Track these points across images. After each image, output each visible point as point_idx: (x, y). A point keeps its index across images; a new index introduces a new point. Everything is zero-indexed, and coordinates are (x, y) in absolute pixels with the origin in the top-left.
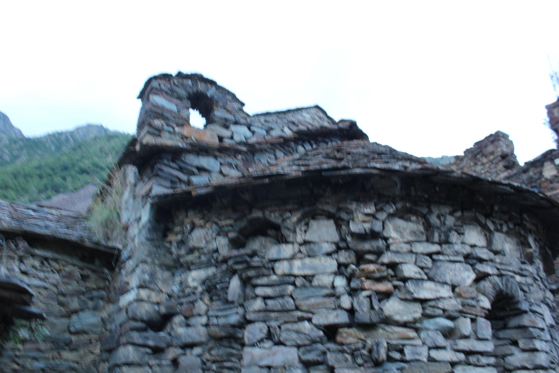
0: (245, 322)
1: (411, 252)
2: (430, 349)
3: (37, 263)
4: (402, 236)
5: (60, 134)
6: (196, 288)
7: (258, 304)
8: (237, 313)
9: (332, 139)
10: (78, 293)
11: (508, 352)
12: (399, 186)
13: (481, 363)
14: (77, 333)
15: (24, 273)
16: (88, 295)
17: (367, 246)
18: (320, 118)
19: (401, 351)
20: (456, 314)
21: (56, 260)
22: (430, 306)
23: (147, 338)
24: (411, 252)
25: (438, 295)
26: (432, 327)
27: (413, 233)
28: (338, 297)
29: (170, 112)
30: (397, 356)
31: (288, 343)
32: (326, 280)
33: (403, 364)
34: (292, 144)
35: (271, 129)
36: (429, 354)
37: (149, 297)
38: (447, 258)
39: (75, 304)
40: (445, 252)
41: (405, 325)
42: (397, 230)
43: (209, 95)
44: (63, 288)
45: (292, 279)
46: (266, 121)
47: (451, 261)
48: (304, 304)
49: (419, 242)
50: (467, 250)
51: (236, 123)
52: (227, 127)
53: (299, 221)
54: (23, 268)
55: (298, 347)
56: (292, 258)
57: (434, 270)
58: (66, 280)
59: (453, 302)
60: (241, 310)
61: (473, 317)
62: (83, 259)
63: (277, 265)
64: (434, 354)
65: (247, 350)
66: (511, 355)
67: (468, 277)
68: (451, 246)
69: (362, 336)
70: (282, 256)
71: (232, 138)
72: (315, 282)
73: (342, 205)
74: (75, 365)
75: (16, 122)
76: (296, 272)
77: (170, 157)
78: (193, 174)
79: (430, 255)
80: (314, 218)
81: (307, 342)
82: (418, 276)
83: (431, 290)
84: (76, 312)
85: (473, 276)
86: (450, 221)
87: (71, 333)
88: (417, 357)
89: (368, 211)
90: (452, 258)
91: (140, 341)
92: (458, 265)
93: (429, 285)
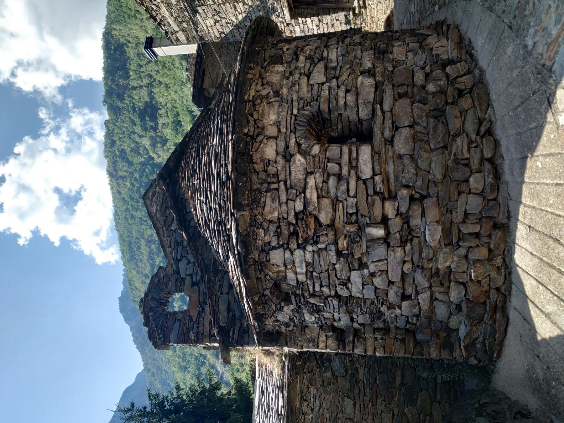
0: (338, 296)
1: (287, 203)
2: (349, 196)
6: (316, 317)
7: (325, 290)
8: (332, 301)
12: (243, 213)
14: (346, 371)
15: (312, 409)
19: (352, 214)
20: (326, 174)
22: (322, 192)
24: (287, 203)
25: (314, 187)
27: (273, 200)
30: (354, 218)
31: (348, 275)
32: (308, 256)
36: (352, 197)
37: (324, 342)
38: (288, 177)
39: (328, 374)
41: (334, 210)
42: (271, 212)
44: (319, 384)
45: (309, 274)
46: (170, 247)
48: (325, 267)
54: (309, 412)
56: (296, 273)
57: (297, 188)
59: (317, 175)
60: (330, 299)
65: (353, 294)
67: (299, 160)
71: (191, 275)
72: (311, 261)
74: (366, 369)
76: (304, 271)
78: (234, 315)
79: (287, 190)
82: (302, 200)
83: (311, 193)
84: (333, 373)
87: (346, 374)
88: (354, 205)
90: (288, 174)
91: (351, 345)
92: (292, 169)
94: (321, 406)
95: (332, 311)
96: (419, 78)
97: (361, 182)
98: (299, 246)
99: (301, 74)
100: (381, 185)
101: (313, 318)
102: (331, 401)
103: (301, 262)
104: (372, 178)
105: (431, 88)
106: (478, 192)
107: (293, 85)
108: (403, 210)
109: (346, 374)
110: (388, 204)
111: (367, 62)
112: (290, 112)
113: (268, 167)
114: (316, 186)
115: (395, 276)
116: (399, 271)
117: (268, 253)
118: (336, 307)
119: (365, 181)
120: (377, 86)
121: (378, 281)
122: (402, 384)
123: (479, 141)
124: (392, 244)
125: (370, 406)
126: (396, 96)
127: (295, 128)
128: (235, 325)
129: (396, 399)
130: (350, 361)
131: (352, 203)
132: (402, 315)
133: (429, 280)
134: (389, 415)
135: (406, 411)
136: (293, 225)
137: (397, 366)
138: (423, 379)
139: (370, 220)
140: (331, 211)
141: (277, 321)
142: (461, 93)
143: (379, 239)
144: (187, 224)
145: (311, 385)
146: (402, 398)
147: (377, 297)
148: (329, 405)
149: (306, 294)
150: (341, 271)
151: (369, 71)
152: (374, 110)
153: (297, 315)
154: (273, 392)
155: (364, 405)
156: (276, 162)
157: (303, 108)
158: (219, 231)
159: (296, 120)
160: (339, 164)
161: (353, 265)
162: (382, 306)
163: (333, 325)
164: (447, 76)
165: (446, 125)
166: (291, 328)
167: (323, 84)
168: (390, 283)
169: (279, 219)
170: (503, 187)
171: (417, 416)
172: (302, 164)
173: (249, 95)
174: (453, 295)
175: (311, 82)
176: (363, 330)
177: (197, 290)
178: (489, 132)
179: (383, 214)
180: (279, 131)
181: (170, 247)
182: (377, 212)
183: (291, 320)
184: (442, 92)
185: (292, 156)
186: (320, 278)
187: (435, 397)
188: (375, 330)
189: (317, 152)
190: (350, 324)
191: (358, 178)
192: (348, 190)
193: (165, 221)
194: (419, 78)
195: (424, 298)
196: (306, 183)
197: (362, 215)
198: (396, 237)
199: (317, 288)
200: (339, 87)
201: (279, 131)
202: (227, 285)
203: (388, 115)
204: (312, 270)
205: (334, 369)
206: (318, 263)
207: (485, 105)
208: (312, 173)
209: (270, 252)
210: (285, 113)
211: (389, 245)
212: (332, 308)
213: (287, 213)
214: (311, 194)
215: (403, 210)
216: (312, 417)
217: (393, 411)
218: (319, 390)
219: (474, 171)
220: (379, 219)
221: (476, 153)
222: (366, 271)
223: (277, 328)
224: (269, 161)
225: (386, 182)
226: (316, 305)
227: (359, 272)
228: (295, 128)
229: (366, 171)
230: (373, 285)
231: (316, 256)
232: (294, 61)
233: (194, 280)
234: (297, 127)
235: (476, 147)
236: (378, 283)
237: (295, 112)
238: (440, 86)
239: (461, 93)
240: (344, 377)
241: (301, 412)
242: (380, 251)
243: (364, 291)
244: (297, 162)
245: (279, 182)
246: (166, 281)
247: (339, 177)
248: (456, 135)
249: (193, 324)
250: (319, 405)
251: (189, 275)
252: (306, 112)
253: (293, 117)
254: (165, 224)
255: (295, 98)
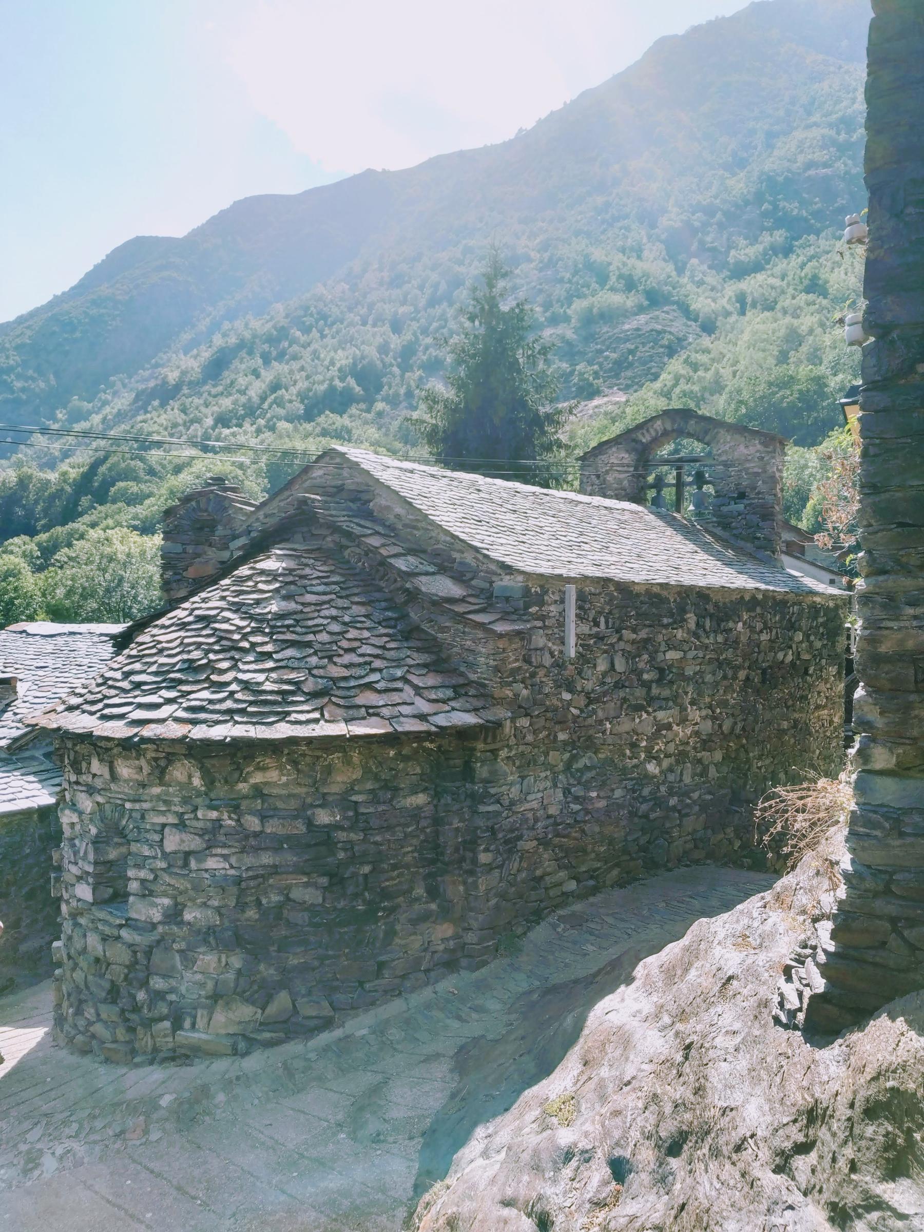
46: (266, 516)
105: (141, 996)
181: (266, 516)
194: (157, 983)
197: (318, 757)
210: (126, 790)
232: (207, 802)
253: (119, 802)
255: (146, 806)
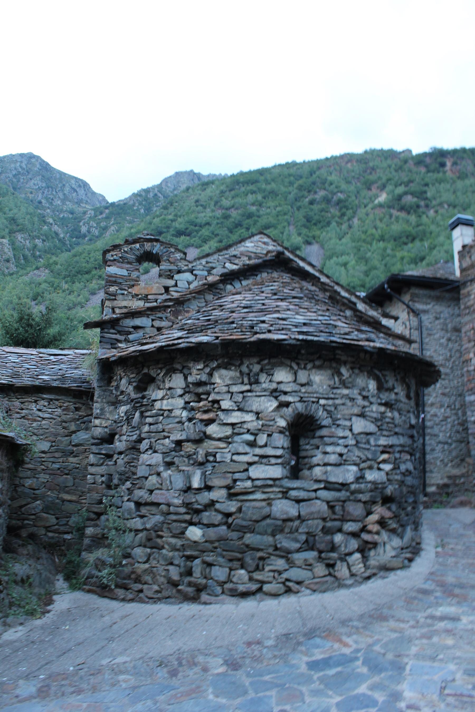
0: (140, 440)
1: (229, 392)
2: (233, 454)
3: (46, 404)
4: (224, 381)
5: (147, 191)
6: (123, 417)
7: (146, 428)
9: (262, 270)
10: (74, 420)
11: (314, 454)
13: (270, 463)
14: (76, 446)
15: (40, 410)
16: (81, 421)
17: (201, 390)
18: (265, 243)
19: (215, 456)
20: (256, 432)
21: (57, 400)
23: (101, 449)
24: (229, 392)
25: (243, 420)
26: (239, 441)
27: (232, 378)
28: (183, 424)
29: (122, 277)
30: (211, 459)
31: (159, 451)
32: (177, 412)
33: (215, 464)
34: (221, 286)
35: (213, 268)
37: (101, 424)
38: (254, 394)
39: (73, 427)
40: (255, 390)
41: (219, 439)
42: (220, 377)
43: (154, 252)
44: (64, 417)
45: (162, 412)
46: (207, 263)
47: (256, 396)
48: (167, 428)
49: (235, 384)
50: (274, 386)
51: (179, 272)
52: (172, 278)
53: (165, 375)
54: (38, 407)
55: (163, 453)
56: (162, 399)
57: (243, 403)
58: (65, 412)
61: (269, 433)
62: (75, 397)
63: (156, 403)
64: (235, 457)
66: (315, 456)
67: (271, 406)
68: (259, 385)
69: (194, 447)
70: (157, 398)
71: (176, 285)
72: (173, 415)
73: (185, 365)
75: (96, 188)
76: (164, 408)
77: (110, 326)
78: (130, 333)
79: (242, 392)
80: (174, 373)
81: (168, 451)
82: (231, 408)
83: (237, 417)
85: (275, 404)
86: (256, 368)
87: (73, 446)
88: (224, 460)
89: (199, 367)
90: (258, 394)
91: (97, 451)
93: (238, 414)
94: (43, 419)
95: (127, 434)
96: (350, 527)
97: (246, 466)
98: (187, 403)
99: (364, 407)
100: (241, 487)
101: (122, 415)
102: (47, 429)
103: (172, 405)
104: (249, 478)
106: (231, 577)
107: (352, 400)
108: (218, 506)
109: (73, 446)
110: (224, 492)
111: (373, 476)
112: (321, 396)
113: (266, 373)
114: (244, 422)
115: (157, 497)
116: (161, 501)
117: (181, 372)
118: (131, 438)
119: (247, 470)
120: (344, 486)
121: (153, 479)
122: (63, 501)
123: (280, 580)
124: (186, 494)
125: (43, 467)
126: (332, 504)
127: (305, 402)
128: (121, 335)
129: (49, 493)
130: (86, 449)
131: (226, 458)
132: (123, 502)
133: (152, 528)
134: (34, 486)
135: (38, 502)
136: (208, 398)
137: (80, 496)
138: (68, 521)
139: (210, 474)
140: (219, 436)
141: (121, 379)
142: (331, 566)
143: (190, 482)
144: (229, 282)
145: (64, 410)
146: (50, 499)
147: (138, 479)
148: (44, 427)
149: (143, 409)
150: (163, 445)
151: (362, 477)
152: (319, 481)
153: (125, 399)
154: (60, 369)
155: (44, 461)
156: (270, 381)
157: (325, 410)
158: (209, 320)
159: (313, 402)
160: (266, 445)
161: (168, 456)
162: (131, 483)
163: (116, 434)
164: (350, 554)
165: (298, 551)
166: (114, 392)
167: (351, 430)
168: (151, 492)
169: (214, 384)
170: (234, 599)
171: (33, 512)
172: (267, 408)
173: (341, 355)
174: (138, 550)
175: (354, 418)
176: (110, 463)
177: (160, 292)
178: (289, 591)
179: (214, 487)
180: (302, 385)
181: (207, 263)
182: (216, 482)
183: (122, 392)
184: (333, 548)
185: (276, 398)
186: (157, 423)
187: (50, 531)
188: (110, 476)
189: (278, 424)
190: (116, 452)
191: (250, 464)
192: (238, 454)
193: (235, 256)
195: (137, 523)
196: (247, 412)
198: (191, 498)
199: (149, 420)
200: (346, 446)
201: (302, 385)
202: (161, 326)
203: (313, 495)
204: (165, 415)
205: (78, 433)
206: (170, 422)
207: (315, 587)
208: (258, 418)
209: (182, 375)
211: (185, 491)
212: (131, 434)
213: (219, 393)
214: (235, 417)
215: (218, 506)
216: (33, 410)
217: (38, 489)
218: (58, 418)
219: (251, 574)
220: (209, 483)
221: (268, 577)
222: (161, 469)
223: (115, 378)
224: (272, 375)
225: (243, 490)
226: (133, 418)
227: (162, 462)
228: (305, 402)
229: (255, 472)
230: (150, 475)
231: (177, 420)
233: (171, 289)
234: (306, 403)
235: (274, 577)
236: (151, 480)
237: (322, 402)
238: (340, 546)
239: (331, 566)
240: (71, 442)
241: (38, 399)
242: (179, 483)
243: (144, 467)
244: (269, 403)
245: (251, 384)
246: (170, 259)
247: (252, 444)
248: (288, 560)
249: (125, 290)
250: (44, 417)
251: (176, 283)
252: (320, 413)
254: (232, 256)
255: (337, 402)
